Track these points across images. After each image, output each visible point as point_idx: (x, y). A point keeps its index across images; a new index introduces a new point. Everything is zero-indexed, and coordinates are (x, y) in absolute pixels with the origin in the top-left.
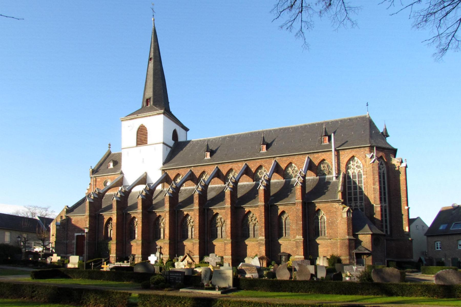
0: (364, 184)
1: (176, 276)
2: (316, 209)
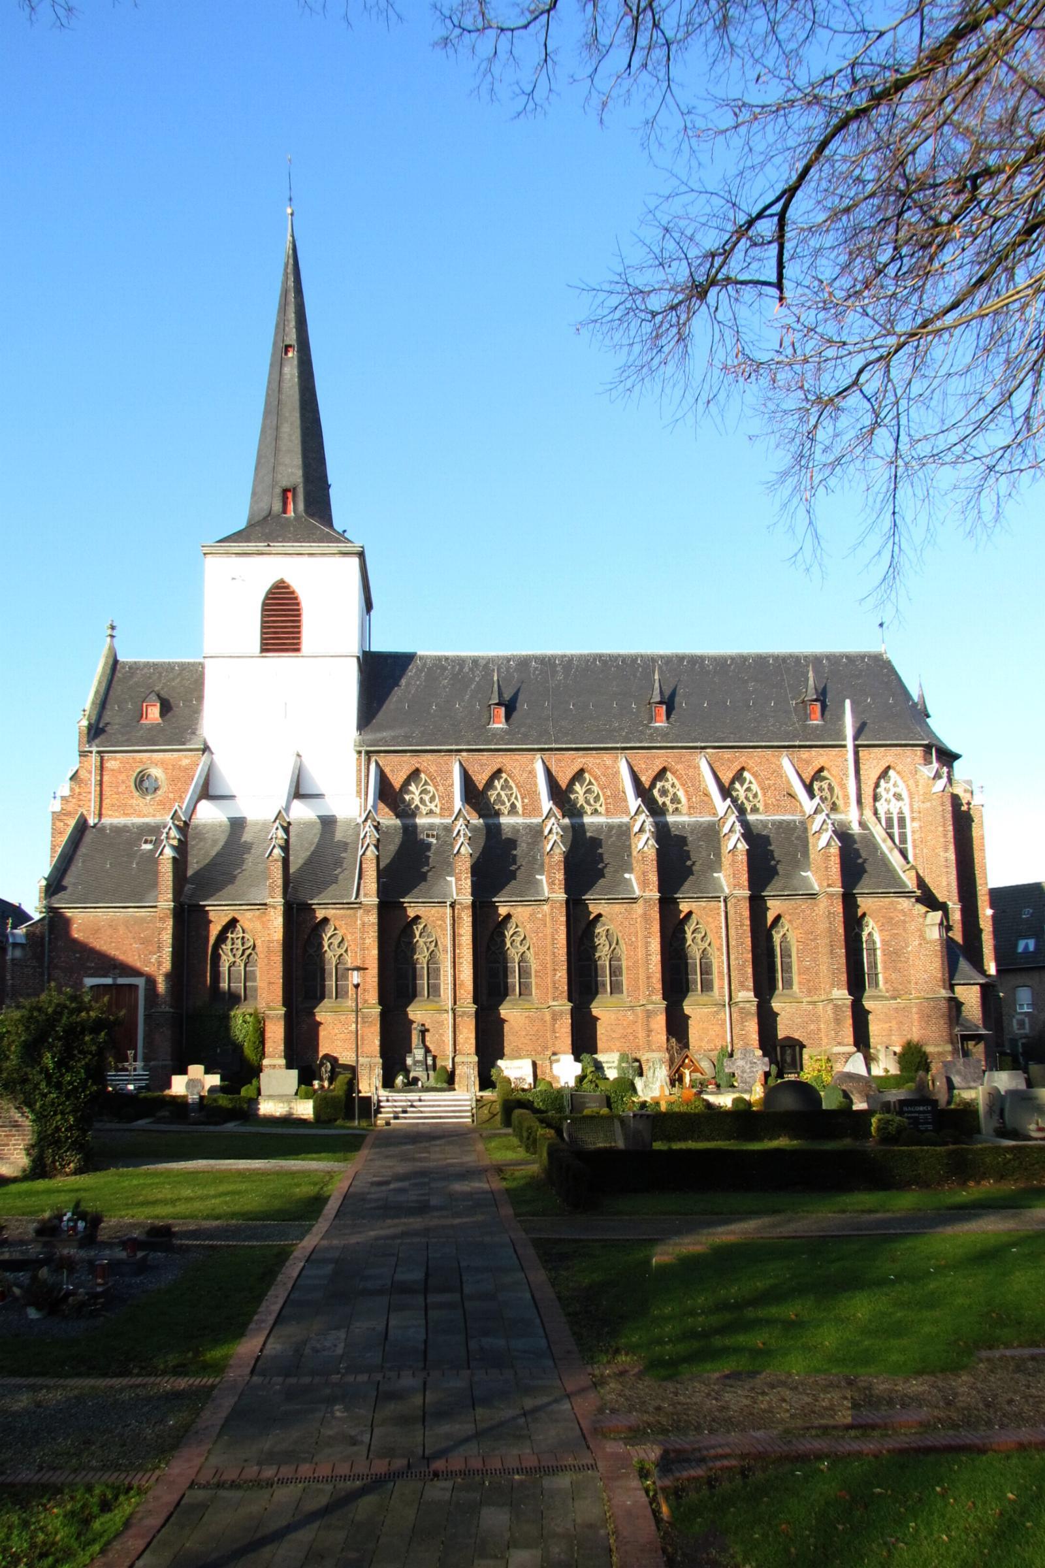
0: (915, 847)
1: (920, 1112)
2: (860, 913)
